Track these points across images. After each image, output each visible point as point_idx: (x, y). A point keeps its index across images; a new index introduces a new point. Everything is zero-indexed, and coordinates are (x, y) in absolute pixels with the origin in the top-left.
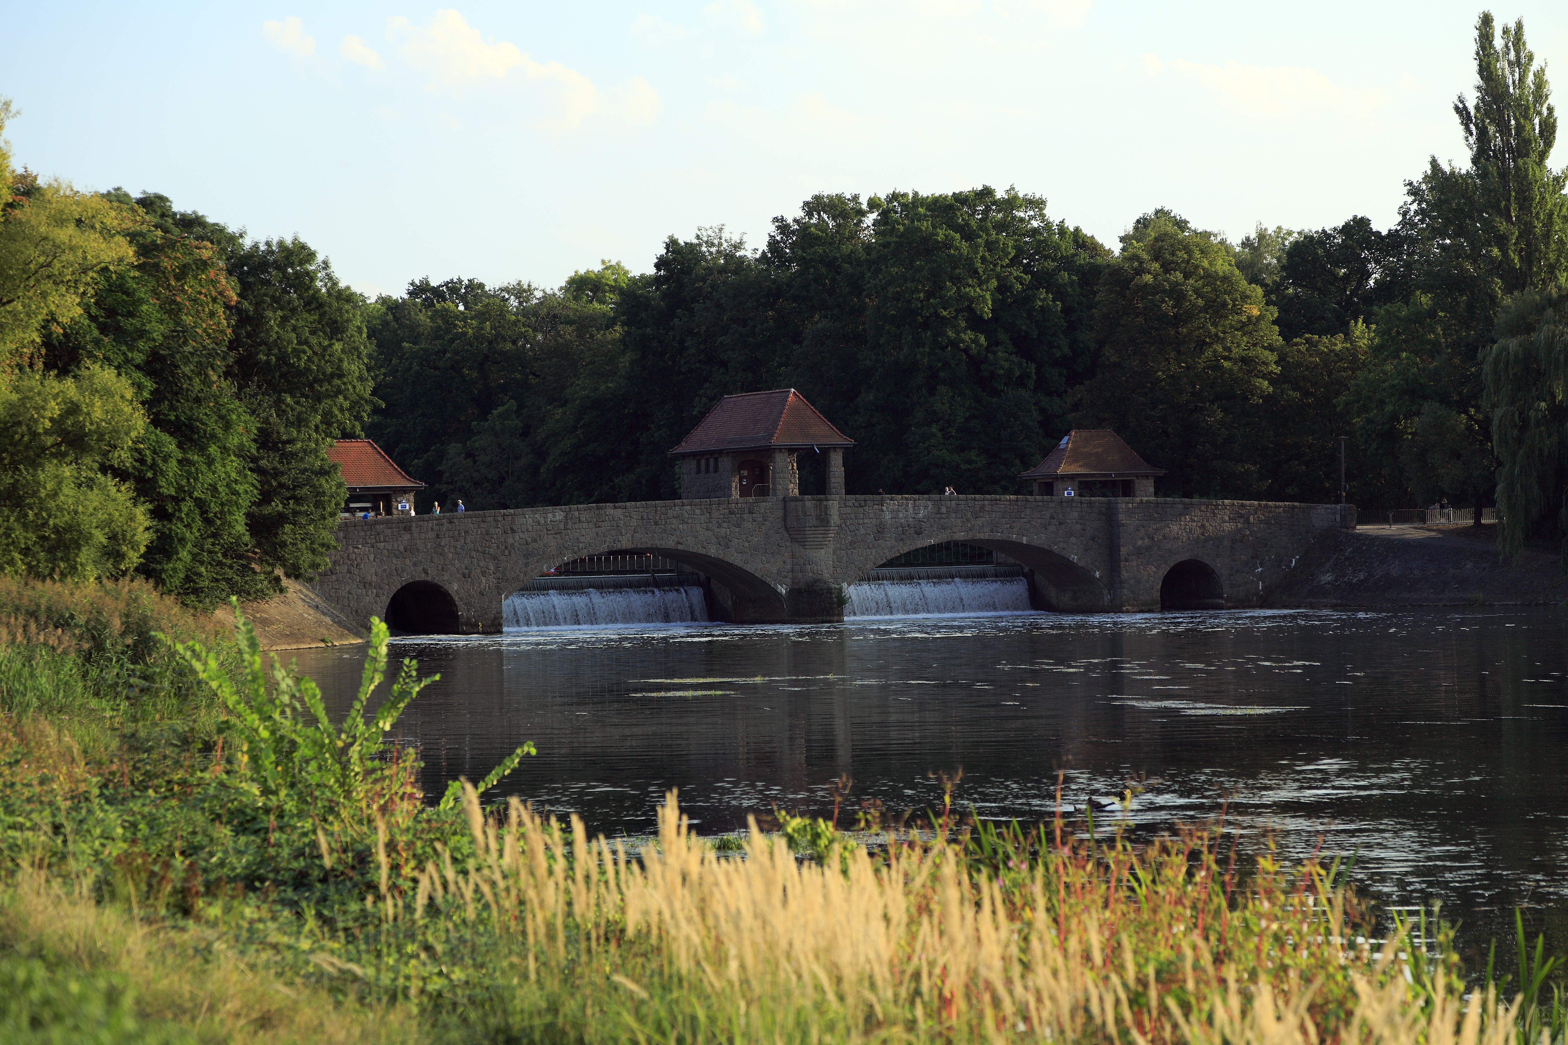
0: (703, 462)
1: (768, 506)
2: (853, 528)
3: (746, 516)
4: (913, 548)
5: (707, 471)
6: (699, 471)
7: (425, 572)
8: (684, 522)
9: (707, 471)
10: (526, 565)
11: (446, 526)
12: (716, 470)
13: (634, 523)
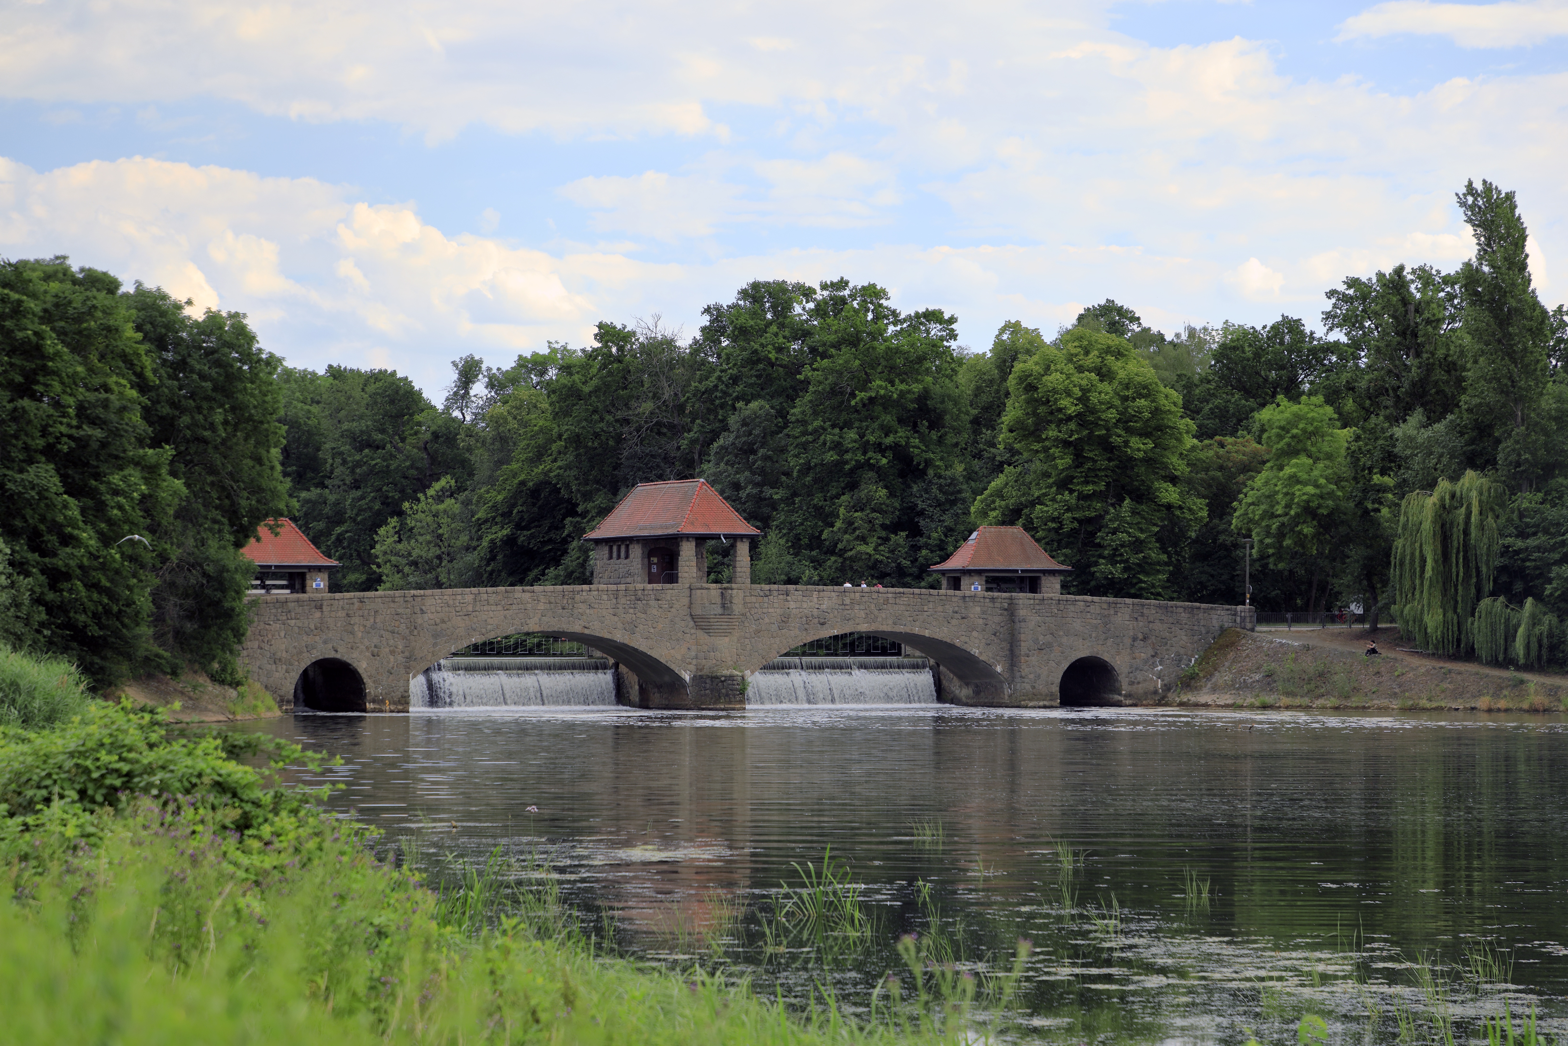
0: (615, 548)
1: (670, 591)
2: (756, 616)
4: (816, 638)
5: (619, 557)
6: (611, 558)
9: (619, 557)
10: (435, 645)
11: (357, 605)
12: (627, 557)
13: (541, 606)
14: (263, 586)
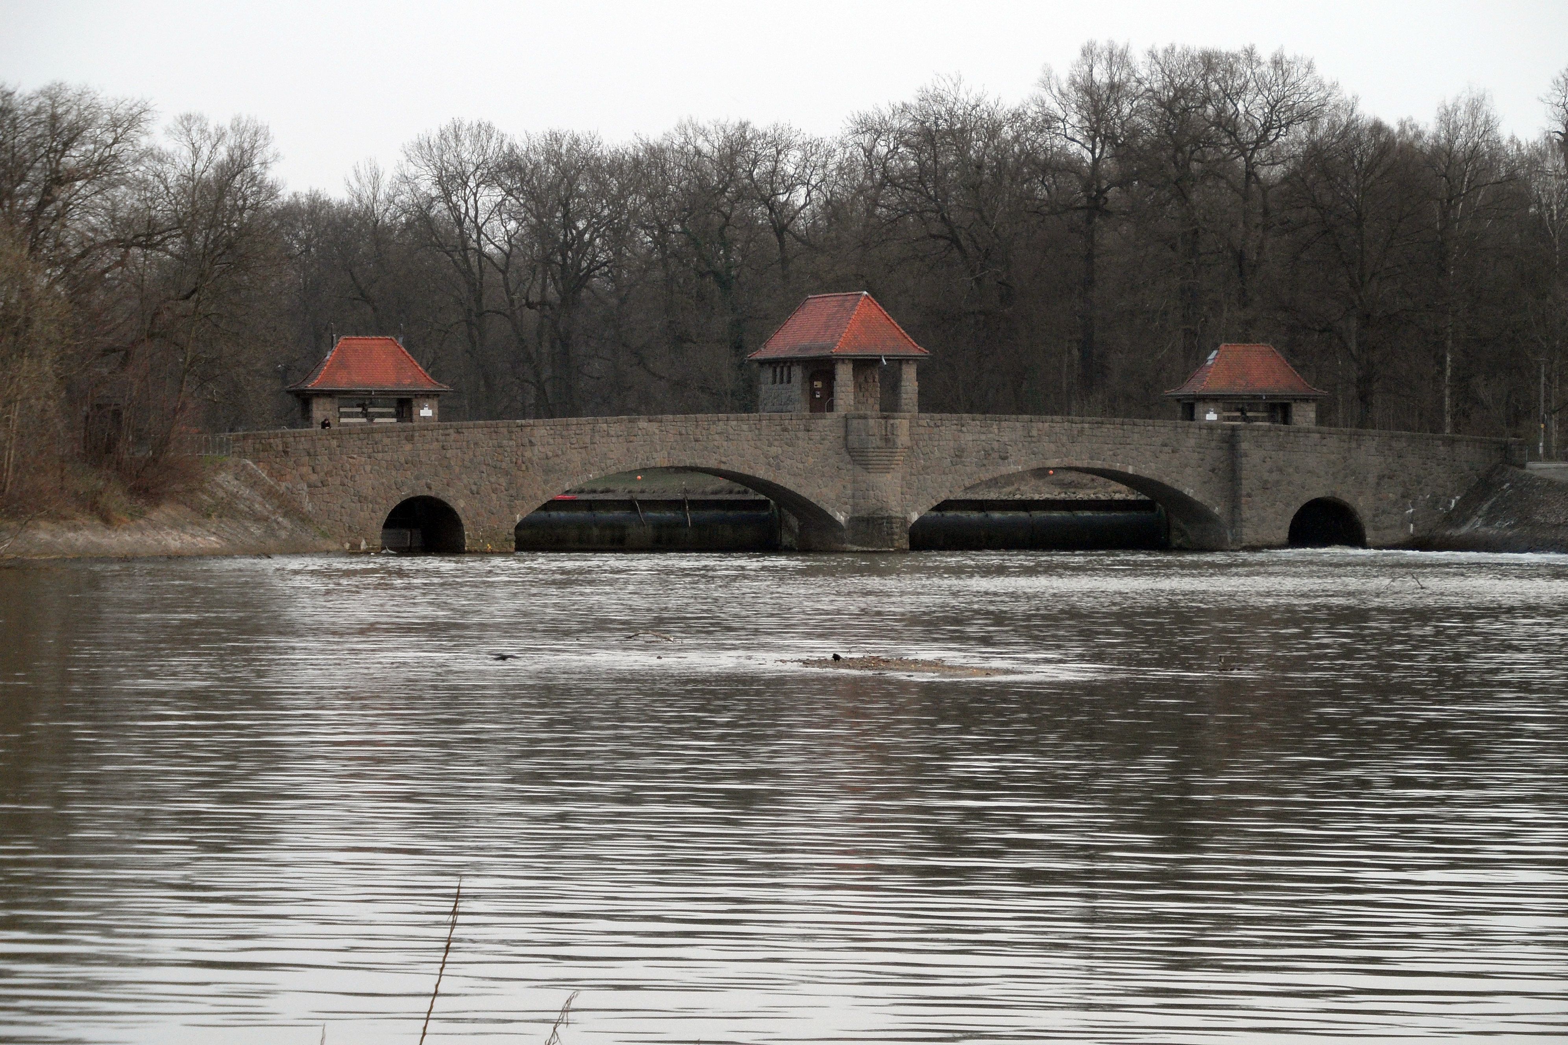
0: (778, 370)
1: (828, 422)
6: (774, 382)
8: (728, 439)
9: (782, 382)
12: (789, 382)
14: (365, 415)
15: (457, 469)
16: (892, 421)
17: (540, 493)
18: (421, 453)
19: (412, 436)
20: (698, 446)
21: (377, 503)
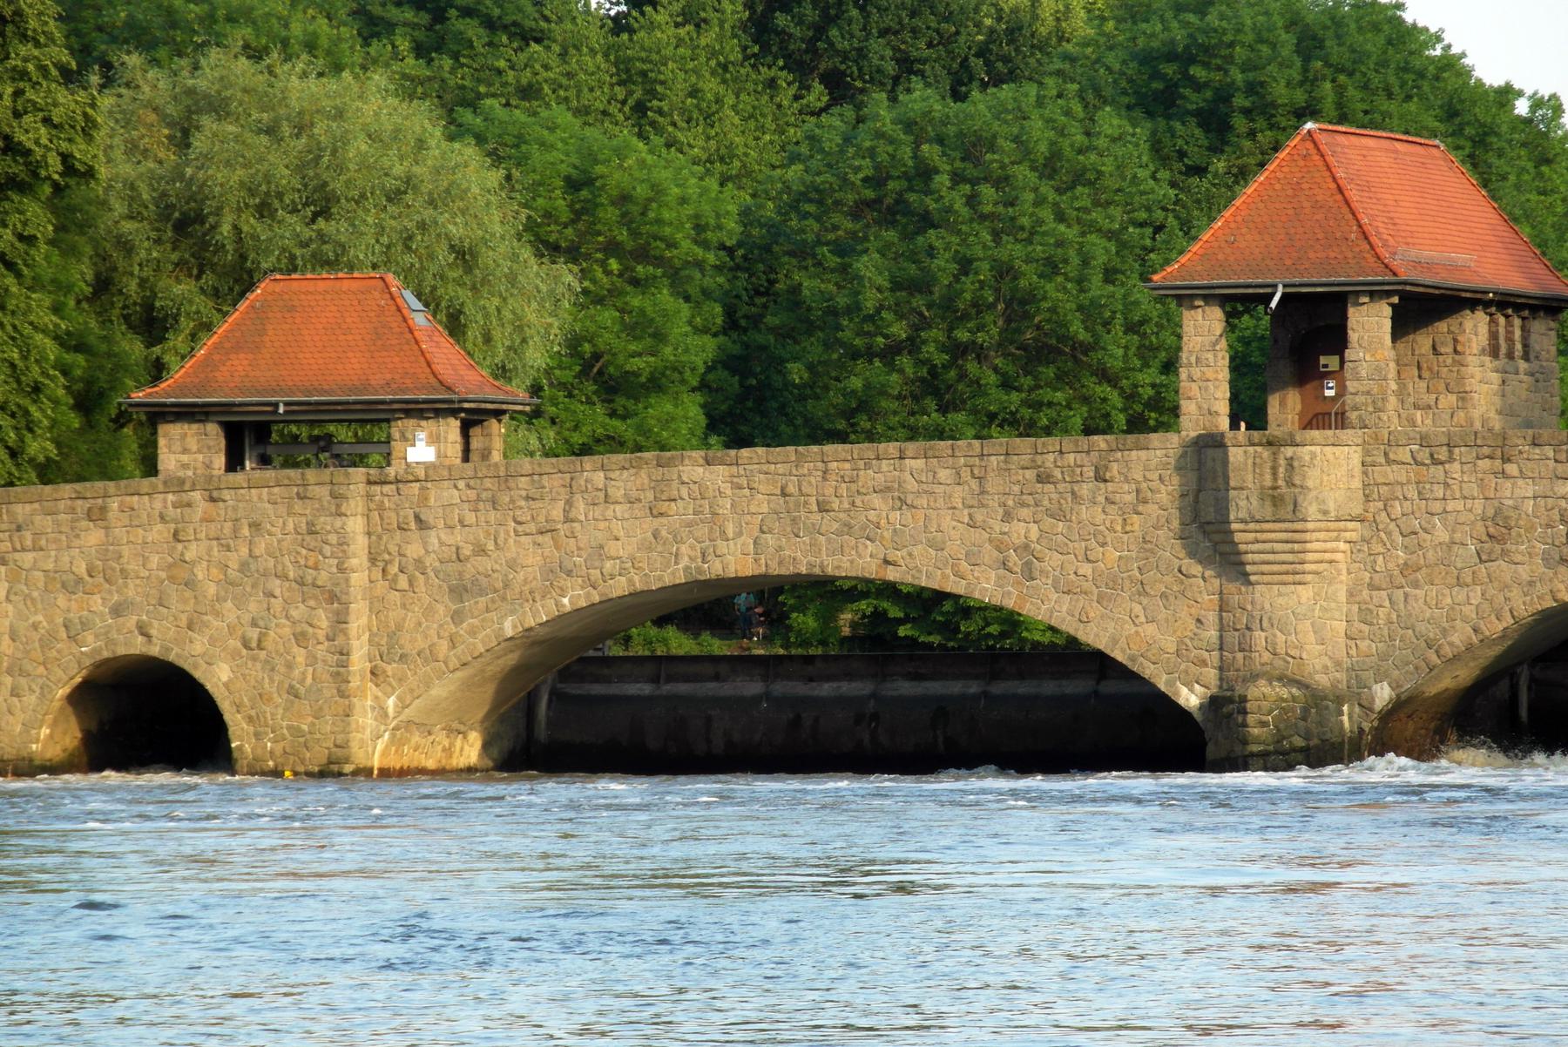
3: (1085, 490)
7: (143, 631)
10: (457, 617)
15: (212, 589)
16: (1289, 451)
17: (443, 647)
18: (126, 551)
19: (103, 509)
20: (829, 524)
21: (23, 673)
